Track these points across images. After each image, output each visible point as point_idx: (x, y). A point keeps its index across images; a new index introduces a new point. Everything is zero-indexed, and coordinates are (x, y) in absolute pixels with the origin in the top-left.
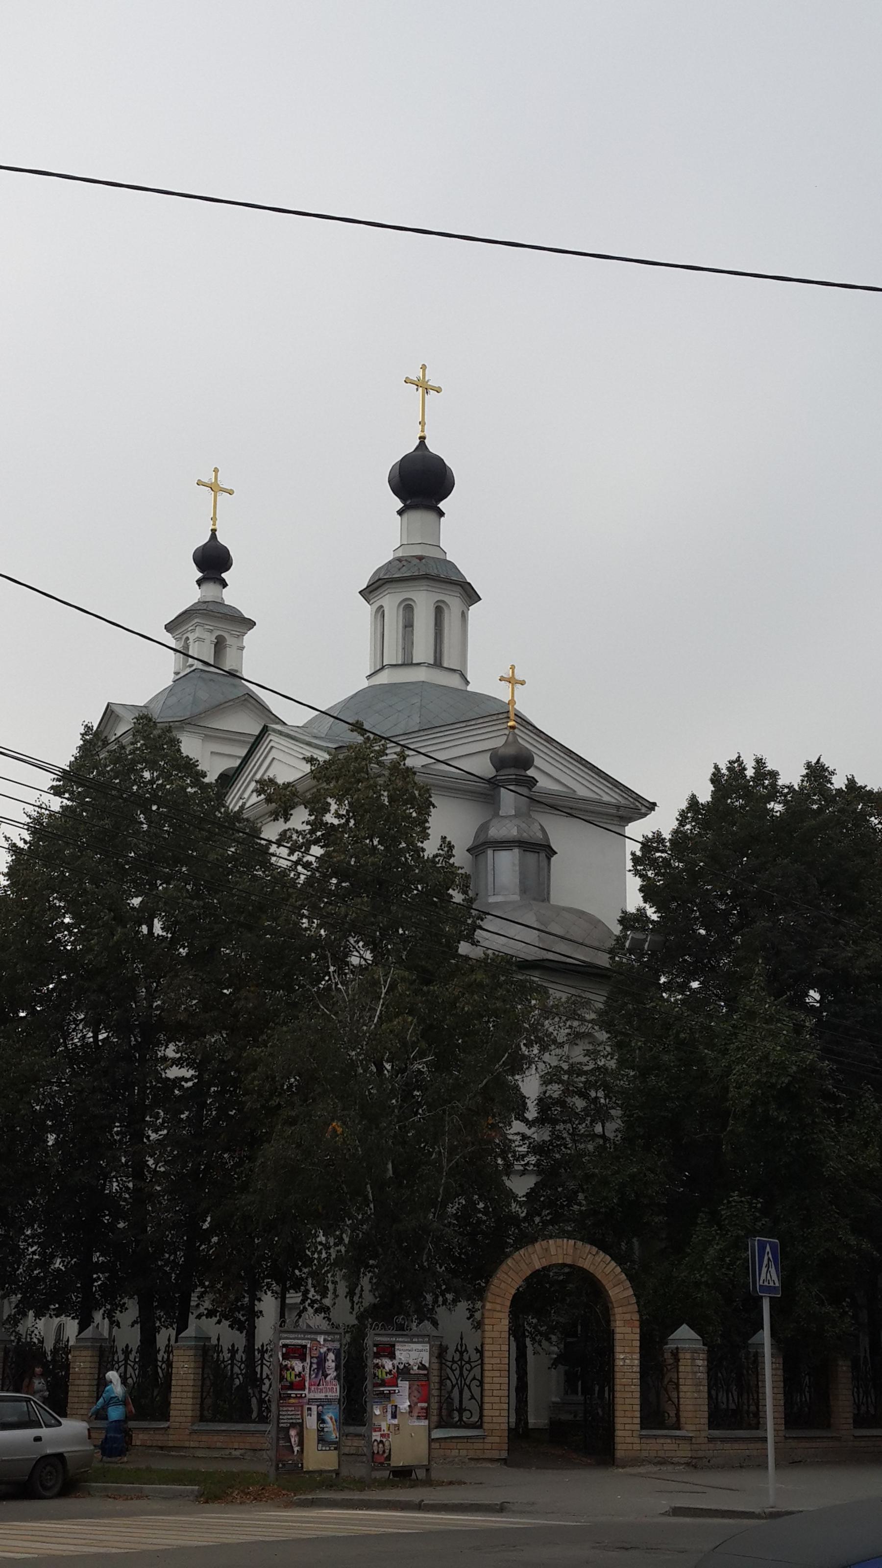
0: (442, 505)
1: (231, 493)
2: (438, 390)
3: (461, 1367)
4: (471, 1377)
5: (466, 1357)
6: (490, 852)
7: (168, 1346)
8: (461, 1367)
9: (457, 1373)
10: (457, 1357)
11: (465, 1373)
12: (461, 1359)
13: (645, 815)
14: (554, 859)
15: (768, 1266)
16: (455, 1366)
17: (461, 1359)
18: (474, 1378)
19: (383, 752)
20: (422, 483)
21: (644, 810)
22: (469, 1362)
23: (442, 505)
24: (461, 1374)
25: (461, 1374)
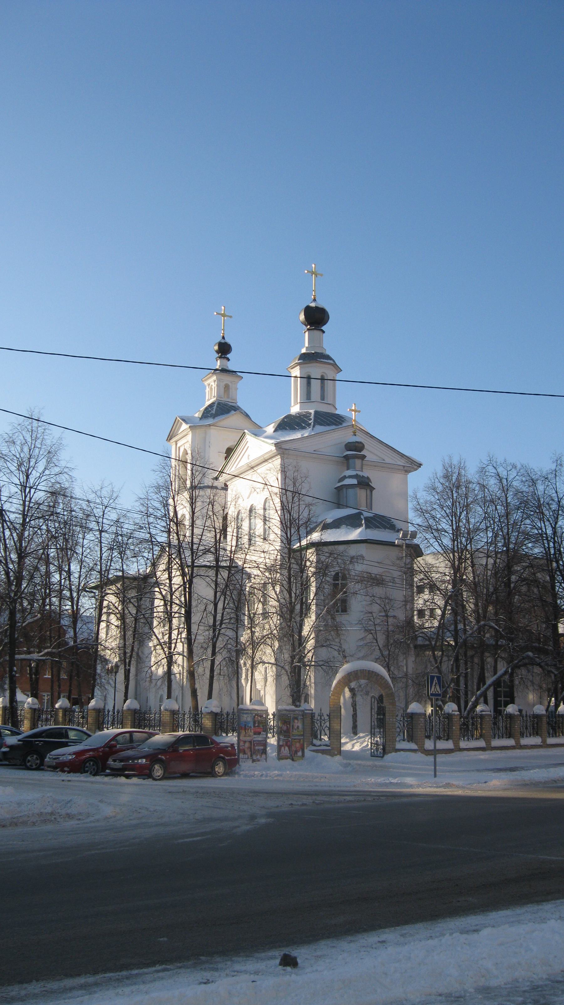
0: (323, 328)
1: (231, 317)
2: (321, 275)
3: (321, 722)
4: (325, 726)
5: (323, 718)
6: (344, 490)
7: (233, 712)
8: (321, 722)
9: (319, 725)
10: (319, 718)
11: (322, 724)
12: (321, 718)
13: (416, 469)
14: (374, 492)
15: (435, 685)
16: (318, 722)
17: (321, 718)
18: (326, 727)
19: (198, 725)
20: (316, 318)
21: (416, 467)
22: (324, 720)
23: (323, 328)
24: (321, 725)
25: (321, 725)
